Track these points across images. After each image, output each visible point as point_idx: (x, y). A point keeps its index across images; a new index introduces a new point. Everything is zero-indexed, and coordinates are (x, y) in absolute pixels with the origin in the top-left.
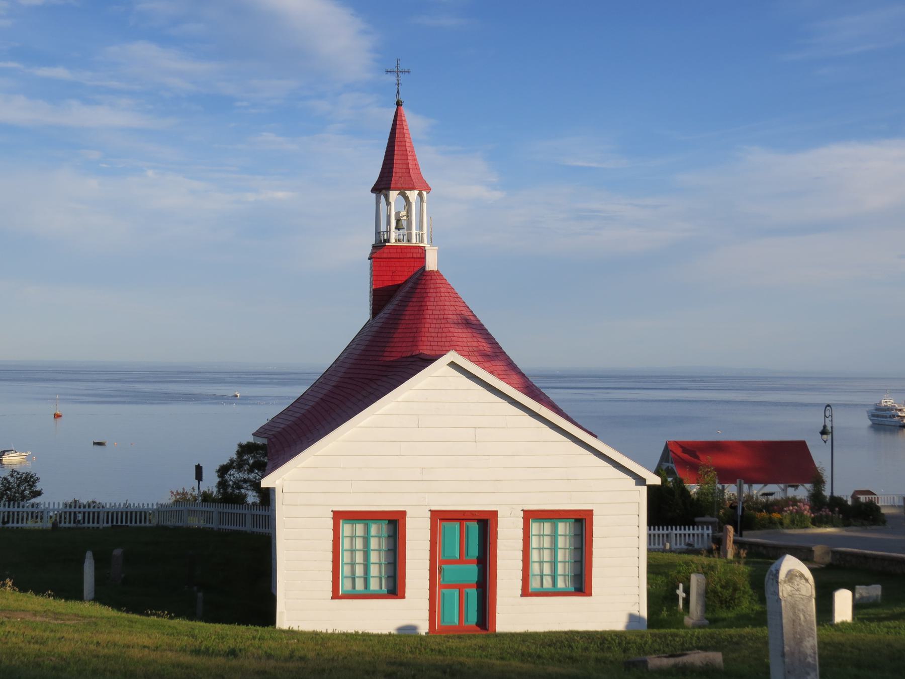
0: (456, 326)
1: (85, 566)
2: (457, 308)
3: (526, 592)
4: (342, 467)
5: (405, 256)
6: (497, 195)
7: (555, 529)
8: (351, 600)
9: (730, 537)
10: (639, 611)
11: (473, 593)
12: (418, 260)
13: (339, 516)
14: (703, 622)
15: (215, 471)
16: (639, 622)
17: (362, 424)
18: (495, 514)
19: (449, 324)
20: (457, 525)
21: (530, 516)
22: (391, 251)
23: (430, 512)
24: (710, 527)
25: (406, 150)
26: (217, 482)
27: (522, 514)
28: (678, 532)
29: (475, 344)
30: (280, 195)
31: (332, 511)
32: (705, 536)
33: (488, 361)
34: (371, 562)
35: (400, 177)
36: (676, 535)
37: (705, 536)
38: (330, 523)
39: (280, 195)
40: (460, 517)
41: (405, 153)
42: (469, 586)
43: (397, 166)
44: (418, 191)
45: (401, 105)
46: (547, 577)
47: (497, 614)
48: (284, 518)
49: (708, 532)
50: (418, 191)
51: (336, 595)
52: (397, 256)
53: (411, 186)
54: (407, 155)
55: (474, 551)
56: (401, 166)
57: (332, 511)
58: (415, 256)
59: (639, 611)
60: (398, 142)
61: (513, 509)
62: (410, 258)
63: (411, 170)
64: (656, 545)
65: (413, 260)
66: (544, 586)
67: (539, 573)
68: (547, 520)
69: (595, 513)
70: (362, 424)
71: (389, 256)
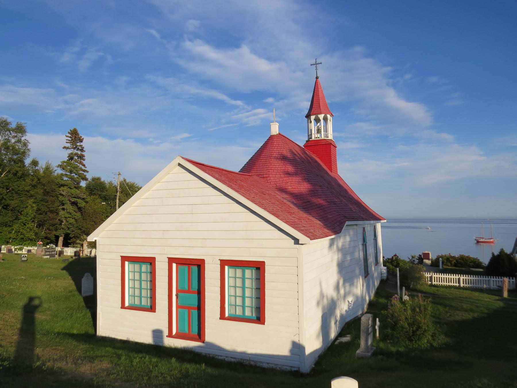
0: (275, 160)
1: (82, 280)
2: (280, 151)
3: (222, 317)
4: (125, 230)
5: (318, 144)
6: (484, 158)
7: (243, 274)
8: (130, 310)
9: (506, 285)
10: (299, 341)
11: (195, 312)
12: (324, 145)
13: (124, 259)
14: (365, 353)
15: (470, 255)
16: (299, 349)
17: (135, 204)
18: (203, 261)
19: (272, 161)
20: (186, 268)
21: (224, 263)
22: (312, 142)
23: (167, 259)
24: (514, 278)
25: (319, 98)
26: (478, 258)
27: (219, 262)
28: (495, 279)
29: (283, 168)
30: (405, 164)
31: (121, 256)
32: (511, 282)
33: (287, 177)
34: (142, 288)
35: (316, 109)
36: (493, 281)
37: (511, 282)
38: (120, 262)
39: (405, 164)
40: (181, 262)
41: (318, 99)
42: (193, 308)
43: (315, 105)
44: (324, 115)
45: (318, 78)
46: (233, 306)
47: (206, 329)
48: (100, 259)
49: (513, 280)
50: (324, 115)
51: (123, 307)
52: (314, 144)
53: (320, 112)
54: (319, 99)
55: (195, 287)
56: (316, 105)
57: (121, 256)
58: (322, 144)
59: (299, 341)
60: (315, 94)
61: (214, 258)
62: (320, 145)
63: (321, 106)
64: (475, 284)
65: (322, 145)
66: (237, 314)
67: (234, 304)
68: (238, 267)
69: (266, 264)
70: (135, 204)
71: (311, 145)
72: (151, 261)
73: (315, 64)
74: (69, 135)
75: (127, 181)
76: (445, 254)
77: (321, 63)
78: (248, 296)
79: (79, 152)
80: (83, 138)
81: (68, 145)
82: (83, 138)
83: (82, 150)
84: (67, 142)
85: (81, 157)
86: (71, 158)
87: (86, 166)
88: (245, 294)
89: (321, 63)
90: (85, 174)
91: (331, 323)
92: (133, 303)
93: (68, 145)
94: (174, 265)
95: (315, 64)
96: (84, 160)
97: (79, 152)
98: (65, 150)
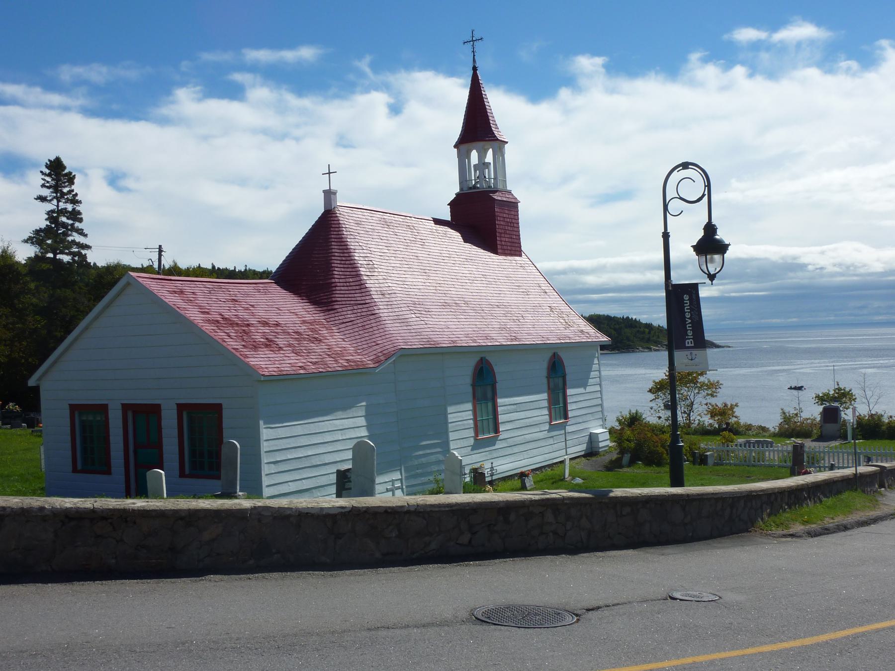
57: (176, 404)
72: (154, 410)
73: (471, 41)
74: (47, 171)
75: (201, 266)
76: (87, 233)
77: (481, 39)
78: (599, 387)
79: (70, 207)
80: (75, 175)
81: (46, 192)
82: (75, 175)
83: (75, 201)
84: (43, 186)
85: (75, 215)
86: (52, 217)
87: (85, 231)
88: (492, 405)
89: (481, 39)
90: (83, 252)
91: (300, 506)
92: (546, 401)
93: (46, 192)
94: (130, 415)
95: (471, 41)
96: (81, 220)
97: (70, 207)
98: (38, 202)
